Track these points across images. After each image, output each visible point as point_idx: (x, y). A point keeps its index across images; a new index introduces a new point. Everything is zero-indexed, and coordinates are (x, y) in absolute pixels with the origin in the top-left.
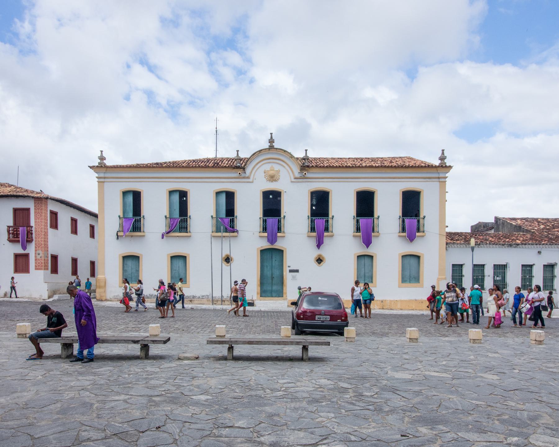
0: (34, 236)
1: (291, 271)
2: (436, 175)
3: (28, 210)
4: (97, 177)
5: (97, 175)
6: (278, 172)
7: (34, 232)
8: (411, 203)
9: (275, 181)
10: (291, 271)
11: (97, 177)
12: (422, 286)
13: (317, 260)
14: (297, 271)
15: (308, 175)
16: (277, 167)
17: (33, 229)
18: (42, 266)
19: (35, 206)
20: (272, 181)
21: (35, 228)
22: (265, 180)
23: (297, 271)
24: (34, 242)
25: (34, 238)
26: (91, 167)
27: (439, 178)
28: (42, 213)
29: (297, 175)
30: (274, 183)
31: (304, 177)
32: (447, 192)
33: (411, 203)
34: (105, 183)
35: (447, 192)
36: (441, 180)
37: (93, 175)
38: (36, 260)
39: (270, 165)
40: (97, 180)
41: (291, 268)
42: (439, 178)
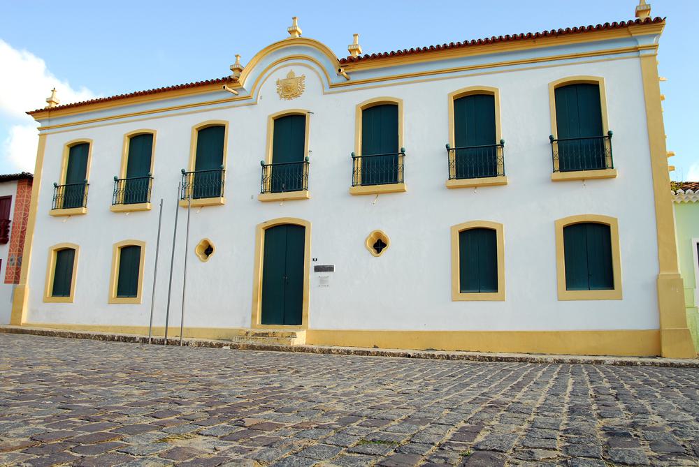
0: (10, 234)
1: (318, 269)
2: (631, 45)
3: (9, 198)
4: (39, 129)
5: (39, 125)
6: (303, 78)
7: (10, 229)
8: (579, 111)
9: (296, 96)
10: (318, 269)
11: (39, 129)
12: (46, 301)
13: (384, 245)
14: (330, 269)
15: (354, 78)
16: (298, 71)
17: (11, 225)
18: (12, 278)
19: (18, 192)
20: (290, 98)
21: (14, 224)
22: (278, 95)
23: (330, 269)
24: (9, 242)
25: (10, 238)
26: (28, 113)
27: (637, 50)
28: (23, 200)
29: (336, 80)
30: (295, 100)
31: (348, 83)
32: (663, 99)
33: (579, 111)
34: (48, 136)
35: (673, 169)
36: (642, 53)
37: (34, 124)
38: (7, 268)
39: (288, 69)
40: (39, 132)
41: (319, 263)
42: (637, 50)
